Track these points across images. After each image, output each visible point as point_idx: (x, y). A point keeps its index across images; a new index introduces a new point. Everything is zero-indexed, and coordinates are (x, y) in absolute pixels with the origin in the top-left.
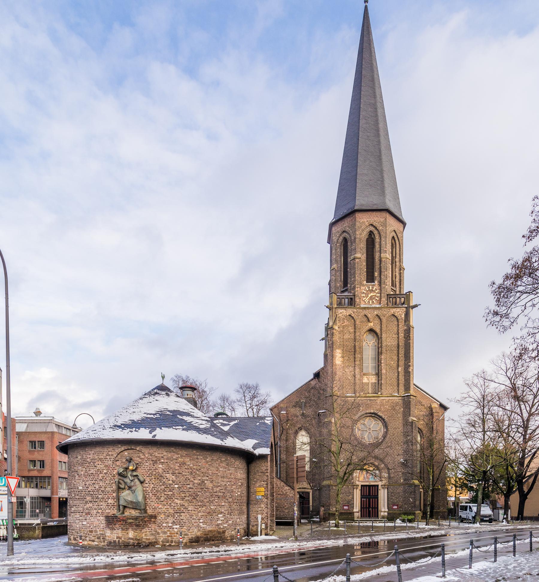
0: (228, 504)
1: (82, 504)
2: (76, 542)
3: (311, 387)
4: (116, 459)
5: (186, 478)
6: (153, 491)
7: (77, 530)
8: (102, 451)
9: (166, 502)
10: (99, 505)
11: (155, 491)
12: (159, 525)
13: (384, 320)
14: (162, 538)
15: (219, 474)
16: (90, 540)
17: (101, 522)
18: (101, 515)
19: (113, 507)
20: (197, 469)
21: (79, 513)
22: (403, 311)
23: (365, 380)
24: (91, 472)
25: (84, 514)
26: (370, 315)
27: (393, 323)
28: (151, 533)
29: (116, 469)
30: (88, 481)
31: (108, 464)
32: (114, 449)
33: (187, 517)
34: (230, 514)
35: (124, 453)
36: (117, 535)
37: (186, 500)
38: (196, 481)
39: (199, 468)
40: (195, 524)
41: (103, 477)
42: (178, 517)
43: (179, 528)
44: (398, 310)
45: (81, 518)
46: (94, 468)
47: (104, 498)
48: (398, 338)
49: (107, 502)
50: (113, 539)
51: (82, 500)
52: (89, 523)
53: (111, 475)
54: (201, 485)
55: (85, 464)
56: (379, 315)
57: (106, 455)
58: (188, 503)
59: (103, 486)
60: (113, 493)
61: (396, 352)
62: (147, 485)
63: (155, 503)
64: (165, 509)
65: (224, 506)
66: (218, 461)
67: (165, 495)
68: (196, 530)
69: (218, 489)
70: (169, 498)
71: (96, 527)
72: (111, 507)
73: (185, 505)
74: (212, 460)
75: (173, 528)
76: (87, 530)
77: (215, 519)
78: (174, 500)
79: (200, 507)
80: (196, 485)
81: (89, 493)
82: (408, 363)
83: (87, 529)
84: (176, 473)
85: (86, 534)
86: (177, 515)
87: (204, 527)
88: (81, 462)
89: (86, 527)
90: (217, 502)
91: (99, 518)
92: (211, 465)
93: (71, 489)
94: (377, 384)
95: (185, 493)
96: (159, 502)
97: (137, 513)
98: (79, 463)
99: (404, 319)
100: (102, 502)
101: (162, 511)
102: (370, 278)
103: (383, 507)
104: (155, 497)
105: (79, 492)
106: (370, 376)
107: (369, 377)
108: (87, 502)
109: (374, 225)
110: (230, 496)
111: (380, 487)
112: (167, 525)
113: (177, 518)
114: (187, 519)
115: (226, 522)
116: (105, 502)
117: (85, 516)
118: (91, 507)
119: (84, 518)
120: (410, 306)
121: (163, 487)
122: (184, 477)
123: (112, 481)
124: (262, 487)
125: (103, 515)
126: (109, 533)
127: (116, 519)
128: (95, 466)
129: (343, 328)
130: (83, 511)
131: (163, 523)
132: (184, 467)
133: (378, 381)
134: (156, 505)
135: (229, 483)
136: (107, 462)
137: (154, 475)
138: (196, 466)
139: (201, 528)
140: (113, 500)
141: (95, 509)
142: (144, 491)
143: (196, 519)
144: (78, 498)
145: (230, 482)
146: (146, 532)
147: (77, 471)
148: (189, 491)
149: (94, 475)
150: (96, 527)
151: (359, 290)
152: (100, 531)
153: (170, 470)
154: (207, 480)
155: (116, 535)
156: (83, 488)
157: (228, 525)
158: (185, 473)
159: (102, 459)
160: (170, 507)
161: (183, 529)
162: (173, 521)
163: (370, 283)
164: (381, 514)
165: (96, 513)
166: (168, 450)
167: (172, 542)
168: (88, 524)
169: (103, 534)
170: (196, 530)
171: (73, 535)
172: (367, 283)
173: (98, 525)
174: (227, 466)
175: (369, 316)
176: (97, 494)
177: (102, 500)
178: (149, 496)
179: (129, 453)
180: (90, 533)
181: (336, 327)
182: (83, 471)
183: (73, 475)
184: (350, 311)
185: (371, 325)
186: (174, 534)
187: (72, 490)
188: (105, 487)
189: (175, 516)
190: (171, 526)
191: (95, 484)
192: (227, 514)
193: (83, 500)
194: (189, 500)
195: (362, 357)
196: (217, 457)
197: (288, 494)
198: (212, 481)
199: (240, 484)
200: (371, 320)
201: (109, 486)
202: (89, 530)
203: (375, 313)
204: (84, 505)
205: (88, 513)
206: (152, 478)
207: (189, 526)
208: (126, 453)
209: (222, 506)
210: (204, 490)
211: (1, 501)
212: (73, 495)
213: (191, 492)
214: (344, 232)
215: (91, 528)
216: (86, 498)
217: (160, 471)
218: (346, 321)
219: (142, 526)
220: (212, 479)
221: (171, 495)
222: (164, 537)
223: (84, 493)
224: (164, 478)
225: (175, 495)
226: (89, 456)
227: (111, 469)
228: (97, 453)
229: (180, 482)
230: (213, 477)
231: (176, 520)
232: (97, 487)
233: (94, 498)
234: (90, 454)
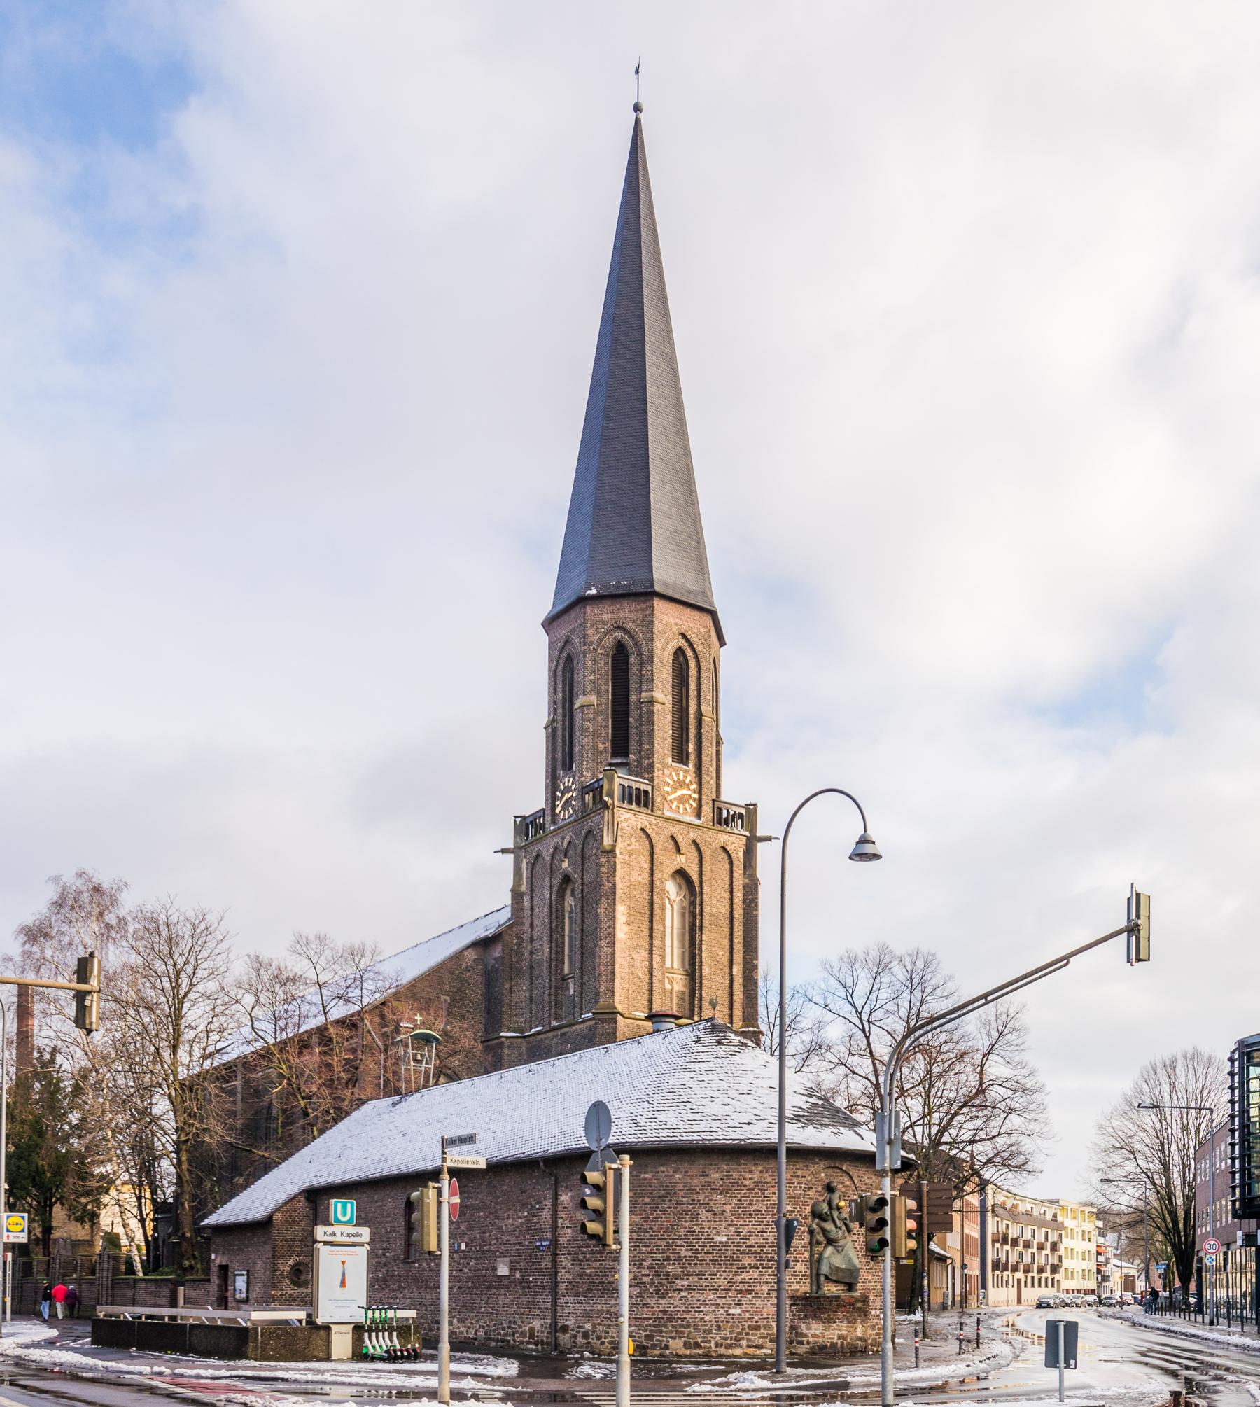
3: (463, 967)
16: (749, 1346)
22: (741, 843)
24: (755, 1208)
29: (808, 1205)
32: (807, 1166)
53: (801, 1215)
56: (698, 841)
82: (752, 960)
99: (742, 860)
106: (675, 976)
109: (689, 637)
120: (756, 836)
127: (836, 1301)
136: (793, 1191)
141: (767, 1283)
151: (661, 775)
155: (836, 1332)
165: (769, 1290)
168: (747, 1314)
175: (680, 839)
179: (826, 1175)
180: (751, 1332)
193: (732, 1264)
200: (683, 850)
203: (692, 834)
210: (739, 1250)
211: (343, 1262)
214: (619, 628)
215: (754, 1320)
218: (633, 840)
226: (750, 1176)
234: (751, 1172)
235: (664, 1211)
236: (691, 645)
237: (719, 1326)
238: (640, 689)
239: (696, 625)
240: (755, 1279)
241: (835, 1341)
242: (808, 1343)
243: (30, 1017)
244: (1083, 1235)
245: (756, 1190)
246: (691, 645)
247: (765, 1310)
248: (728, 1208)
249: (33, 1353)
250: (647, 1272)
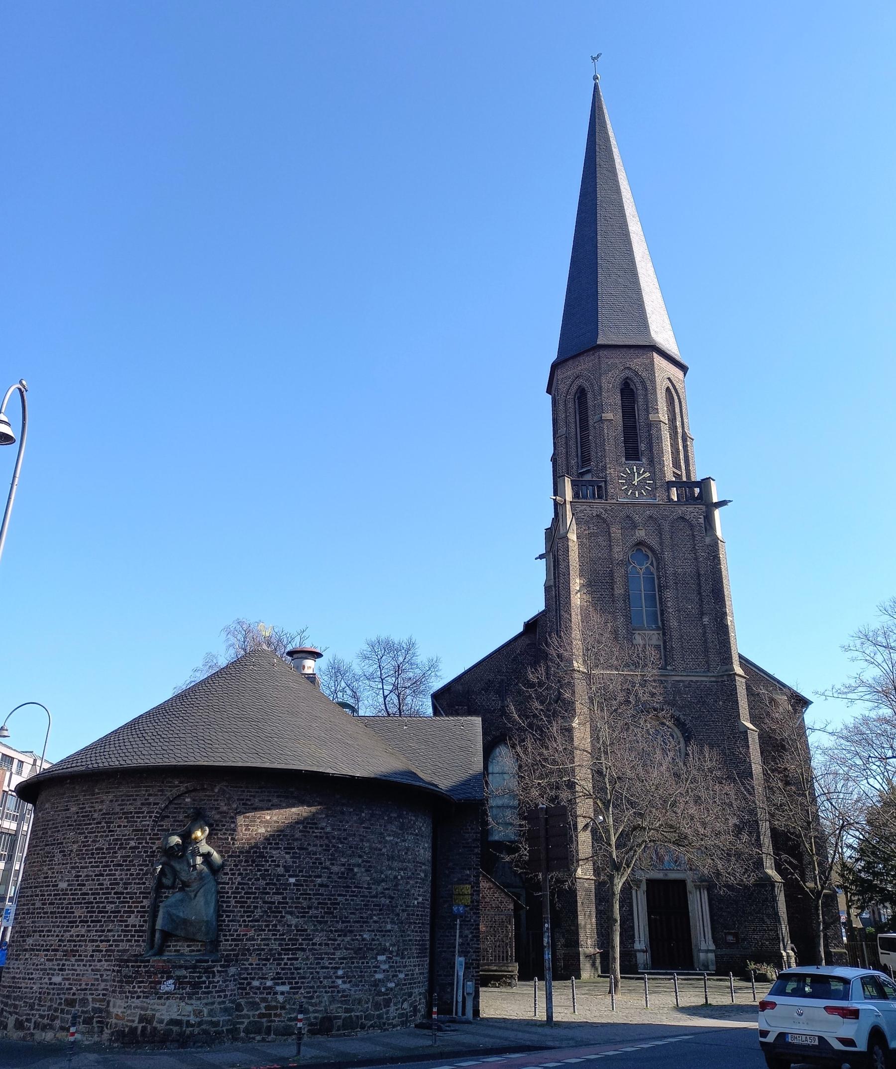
0: (399, 927)
1: (58, 927)
2: (21, 1034)
4: (164, 814)
5: (316, 859)
6: (239, 893)
7: (31, 998)
8: (132, 796)
9: (266, 921)
10: (103, 931)
11: (243, 892)
12: (243, 984)
13: (666, 527)
14: (246, 1021)
15: (384, 850)
17: (102, 975)
18: (103, 956)
19: (139, 936)
20: (339, 839)
21: (48, 950)
26: (637, 516)
27: (684, 533)
28: (222, 1006)
29: (159, 839)
30: (87, 867)
31: (144, 826)
32: (162, 791)
33: (309, 963)
34: (402, 954)
35: (184, 800)
36: (142, 1012)
37: (311, 917)
38: (335, 869)
39: (344, 835)
40: (325, 982)
42: (289, 962)
43: (288, 993)
45: (49, 965)
46: (107, 836)
47: (119, 912)
49: (126, 921)
50: (129, 1024)
51: (61, 917)
52: (68, 979)
53: (146, 852)
54: (346, 878)
55: (86, 824)
57: (142, 804)
58: (315, 926)
59: (122, 879)
60: (144, 898)
62: (226, 879)
63: (240, 926)
64: (262, 940)
65: (389, 931)
66: (383, 819)
67: (265, 902)
68: (325, 998)
69: (380, 889)
70: (274, 910)
71: (86, 989)
72: (133, 936)
73: (306, 930)
74: (372, 815)
75: (276, 993)
76: (62, 999)
77: (369, 967)
78: (284, 917)
79: (339, 936)
80: (335, 877)
81: (84, 899)
83: (62, 996)
84: (294, 848)
85: (56, 1010)
86: (286, 957)
87: (344, 991)
88: (75, 821)
89: (59, 989)
90: (375, 922)
92: (370, 828)
93: (36, 887)
94: (662, 647)
95: (310, 899)
96: (249, 921)
97: (193, 951)
98: (70, 823)
100: (113, 921)
101: (254, 945)
102: (632, 453)
103: (703, 939)
104: (242, 910)
105: (59, 895)
107: (644, 634)
108: (75, 922)
110: (404, 907)
111: (690, 886)
112: (261, 984)
113: (286, 964)
114: (308, 968)
115: (393, 976)
116: (121, 921)
117: (61, 960)
118: (83, 936)
119: (58, 965)
121: (262, 883)
122: (311, 858)
123: (145, 869)
124: (466, 884)
125: (110, 956)
126: (120, 1007)
127: (145, 967)
128: (110, 831)
130: (60, 946)
131: (253, 979)
132: (313, 832)
133: (665, 642)
134: (241, 931)
135: (402, 873)
137: (246, 852)
138: (339, 830)
139: (338, 992)
140: (141, 917)
141: (93, 941)
142: (218, 892)
143: (328, 968)
144: (51, 913)
145: (406, 869)
146: (213, 1003)
147: (62, 843)
148: (318, 894)
149: (104, 853)
150: (86, 989)
153: (281, 840)
154: (359, 866)
155: (139, 1012)
156: (69, 885)
157: (397, 985)
158: (314, 849)
159: (131, 813)
160: (273, 935)
161: (297, 996)
162: (278, 973)
163: (634, 462)
164: (698, 956)
165: (93, 951)
166: (281, 792)
167: (269, 1034)
168: (67, 982)
169: (100, 1011)
170: (325, 998)
171: (16, 1013)
172: (626, 460)
173: (92, 985)
174: (400, 832)
175: (636, 518)
176: (103, 902)
177: (114, 917)
178: (227, 906)
179: (194, 800)
180: (67, 1008)
182: (77, 842)
183: (49, 853)
185: (641, 534)
186: (276, 1008)
187: (38, 890)
188: (125, 884)
189: (283, 959)
190: (270, 988)
191: (102, 875)
192: (395, 954)
193: (65, 917)
194: (317, 917)
195: (629, 595)
196: (383, 810)
197: (487, 900)
198: (370, 866)
199: (422, 875)
201: (137, 881)
202: (66, 1000)
204: (65, 931)
205: (72, 951)
206: (239, 861)
207: (311, 987)
208: (188, 800)
209: (386, 931)
212: (38, 904)
213: (322, 895)
215: (72, 991)
216: (73, 913)
219: (205, 988)
220: (369, 862)
221: (279, 903)
222: (252, 1019)
223: (69, 899)
224: (267, 861)
225: (287, 903)
227: (148, 837)
228: (120, 799)
229: (301, 871)
230: (371, 858)
231: (283, 969)
232: (107, 883)
233: (94, 912)
234: (102, 802)
236: (636, 374)
241: (135, 1025)
245: (103, 824)
247: (85, 978)
249: (693, 999)
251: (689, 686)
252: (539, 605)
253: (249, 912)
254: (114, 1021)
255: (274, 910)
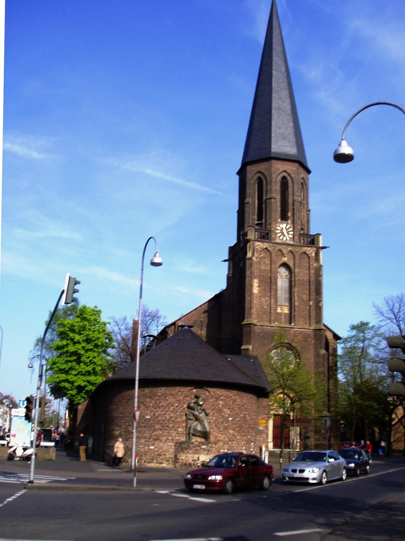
10: (169, 433)
16: (157, 463)
23: (279, 310)
25: (151, 440)
39: (243, 404)
41: (174, 409)
44: (309, 249)
46: (165, 401)
48: (309, 273)
61: (307, 287)
91: (169, 444)
99: (314, 257)
102: (284, 218)
121: (222, 419)
129: (260, 259)
134: (217, 434)
152: (169, 455)
175: (284, 251)
181: (254, 259)
184: (266, 245)
185: (285, 259)
217: (220, 406)
235: (129, 405)
236: (289, 175)
237: (145, 454)
238: (266, 195)
239: (291, 168)
240: (161, 434)
242: (180, 462)
243: (363, 322)
244: (29, 409)
246: (289, 175)
248: (151, 404)
250: (123, 430)
251: (300, 333)
252: (221, 285)
253: (219, 429)
254: (181, 461)
255: (226, 428)
